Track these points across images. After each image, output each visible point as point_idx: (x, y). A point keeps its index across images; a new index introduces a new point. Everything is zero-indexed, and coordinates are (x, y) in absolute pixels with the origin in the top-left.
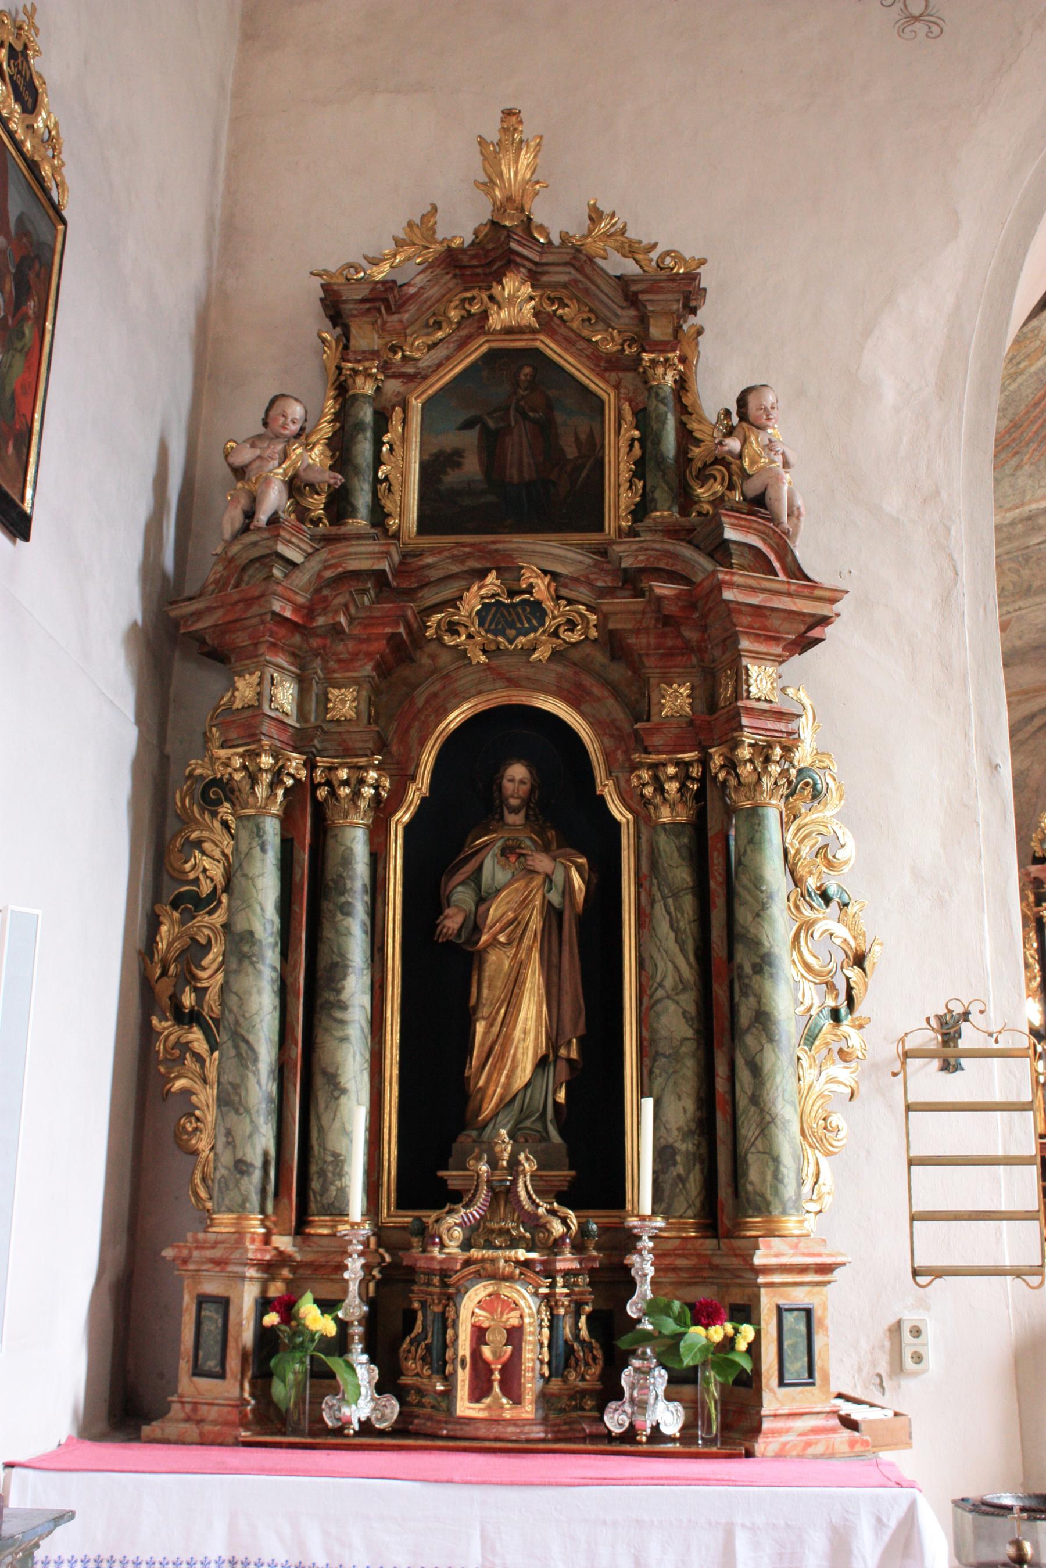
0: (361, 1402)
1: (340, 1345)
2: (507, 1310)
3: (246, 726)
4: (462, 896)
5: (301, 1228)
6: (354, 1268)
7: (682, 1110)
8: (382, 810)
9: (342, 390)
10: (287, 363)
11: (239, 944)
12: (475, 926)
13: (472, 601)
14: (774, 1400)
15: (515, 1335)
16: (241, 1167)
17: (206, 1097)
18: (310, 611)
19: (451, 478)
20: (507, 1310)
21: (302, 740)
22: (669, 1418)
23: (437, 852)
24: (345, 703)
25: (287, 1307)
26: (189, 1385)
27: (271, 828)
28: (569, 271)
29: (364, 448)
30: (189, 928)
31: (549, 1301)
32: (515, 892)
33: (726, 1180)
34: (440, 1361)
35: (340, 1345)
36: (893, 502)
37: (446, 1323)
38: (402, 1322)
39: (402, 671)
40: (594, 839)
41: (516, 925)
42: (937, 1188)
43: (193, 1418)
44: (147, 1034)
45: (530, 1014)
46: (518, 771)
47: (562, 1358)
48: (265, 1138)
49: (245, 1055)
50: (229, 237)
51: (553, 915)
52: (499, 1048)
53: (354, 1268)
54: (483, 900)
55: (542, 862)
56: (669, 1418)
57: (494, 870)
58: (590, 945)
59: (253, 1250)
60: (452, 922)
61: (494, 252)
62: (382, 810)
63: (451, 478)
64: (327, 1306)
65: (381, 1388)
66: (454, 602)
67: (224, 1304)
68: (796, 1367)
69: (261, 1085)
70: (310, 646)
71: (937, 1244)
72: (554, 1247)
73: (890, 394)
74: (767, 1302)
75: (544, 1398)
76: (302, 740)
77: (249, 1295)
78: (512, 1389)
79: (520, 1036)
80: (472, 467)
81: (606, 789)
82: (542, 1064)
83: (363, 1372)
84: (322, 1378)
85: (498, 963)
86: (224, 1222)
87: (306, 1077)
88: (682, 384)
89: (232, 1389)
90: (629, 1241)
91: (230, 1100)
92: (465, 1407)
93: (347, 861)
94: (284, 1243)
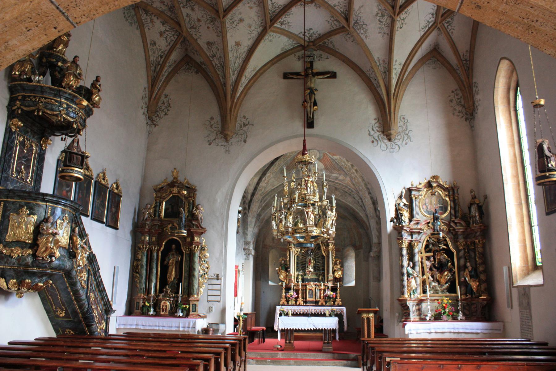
0: (152, 313)
1: (150, 307)
2: (166, 304)
3: (143, 242)
4: (167, 260)
5: (147, 296)
6: (152, 299)
7: (186, 284)
8: (158, 251)
9: (156, 200)
10: (150, 198)
11: (142, 266)
12: (168, 263)
13: (169, 226)
14: (191, 313)
15: (166, 306)
16: (141, 289)
17: (138, 281)
18: (149, 230)
19: (168, 211)
20: (166, 304)
21: (149, 243)
22: (181, 314)
23: (165, 255)
24: (154, 239)
25: (144, 303)
26: (136, 311)
27: (145, 253)
28: (182, 186)
29: (158, 208)
30: (143, 253)
31: (170, 303)
32: (172, 260)
33: (189, 291)
34: (160, 309)
35: (150, 307)
36: (218, 215)
37: (160, 305)
38: (156, 306)
39: (161, 236)
40: (181, 254)
41: (172, 263)
42: (210, 293)
43: (136, 314)
44: (133, 274)
45: (173, 272)
46: (174, 246)
47: (171, 308)
48: (144, 286)
49: (142, 277)
50: (144, 178)
51: (176, 262)
52: (171, 276)
53: (152, 299)
54: (169, 260)
55: (175, 256)
56: (181, 314)
57: (171, 257)
58: (179, 265)
59: (141, 297)
60: (166, 263)
61: (172, 185)
62: (158, 251)
63: (168, 211)
64: (148, 303)
65: (154, 311)
66: (167, 227)
67: (139, 303)
68: (194, 310)
69: (144, 280)
70: (150, 234)
71: (210, 298)
72: (171, 298)
73: (219, 201)
74: (191, 304)
75: (169, 312)
76: (149, 243)
77: (141, 302)
78: (166, 311)
79: (172, 275)
80: (170, 210)
81: (183, 248)
82: (174, 278)
83: (152, 309)
84: (149, 311)
85: (171, 267)
86: (139, 294)
87: (149, 280)
88: (193, 201)
89: (139, 311)
90: (178, 297)
91: (140, 282)
92: (161, 313)
93: (154, 256)
94: (145, 297)
